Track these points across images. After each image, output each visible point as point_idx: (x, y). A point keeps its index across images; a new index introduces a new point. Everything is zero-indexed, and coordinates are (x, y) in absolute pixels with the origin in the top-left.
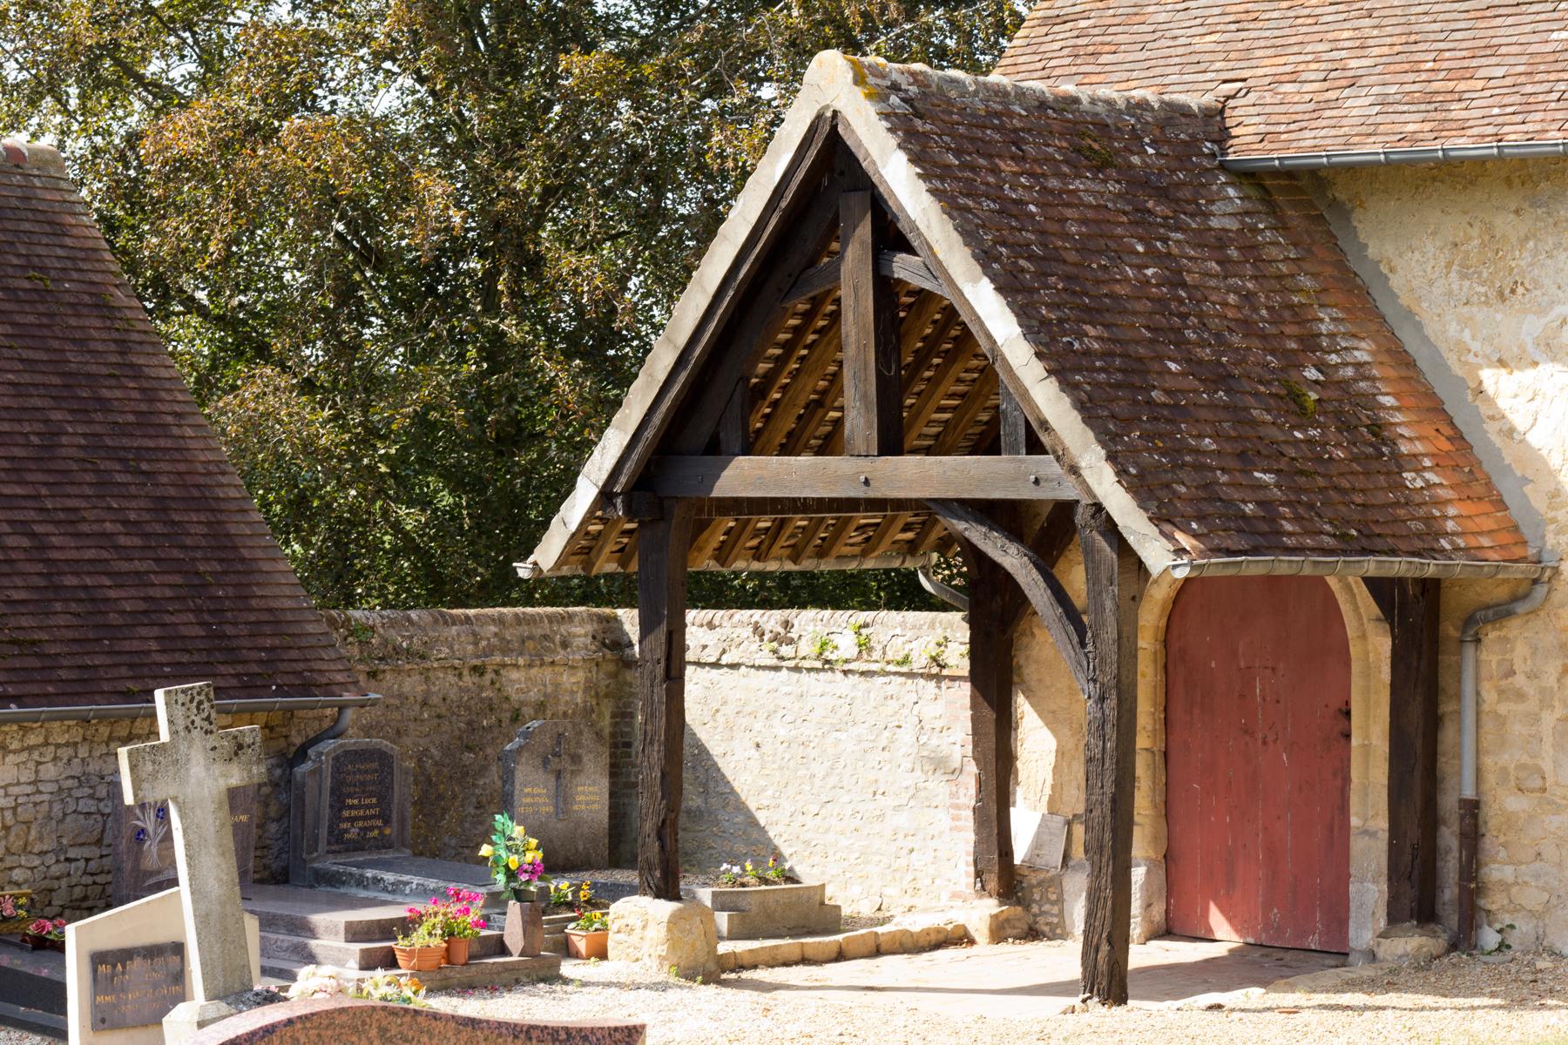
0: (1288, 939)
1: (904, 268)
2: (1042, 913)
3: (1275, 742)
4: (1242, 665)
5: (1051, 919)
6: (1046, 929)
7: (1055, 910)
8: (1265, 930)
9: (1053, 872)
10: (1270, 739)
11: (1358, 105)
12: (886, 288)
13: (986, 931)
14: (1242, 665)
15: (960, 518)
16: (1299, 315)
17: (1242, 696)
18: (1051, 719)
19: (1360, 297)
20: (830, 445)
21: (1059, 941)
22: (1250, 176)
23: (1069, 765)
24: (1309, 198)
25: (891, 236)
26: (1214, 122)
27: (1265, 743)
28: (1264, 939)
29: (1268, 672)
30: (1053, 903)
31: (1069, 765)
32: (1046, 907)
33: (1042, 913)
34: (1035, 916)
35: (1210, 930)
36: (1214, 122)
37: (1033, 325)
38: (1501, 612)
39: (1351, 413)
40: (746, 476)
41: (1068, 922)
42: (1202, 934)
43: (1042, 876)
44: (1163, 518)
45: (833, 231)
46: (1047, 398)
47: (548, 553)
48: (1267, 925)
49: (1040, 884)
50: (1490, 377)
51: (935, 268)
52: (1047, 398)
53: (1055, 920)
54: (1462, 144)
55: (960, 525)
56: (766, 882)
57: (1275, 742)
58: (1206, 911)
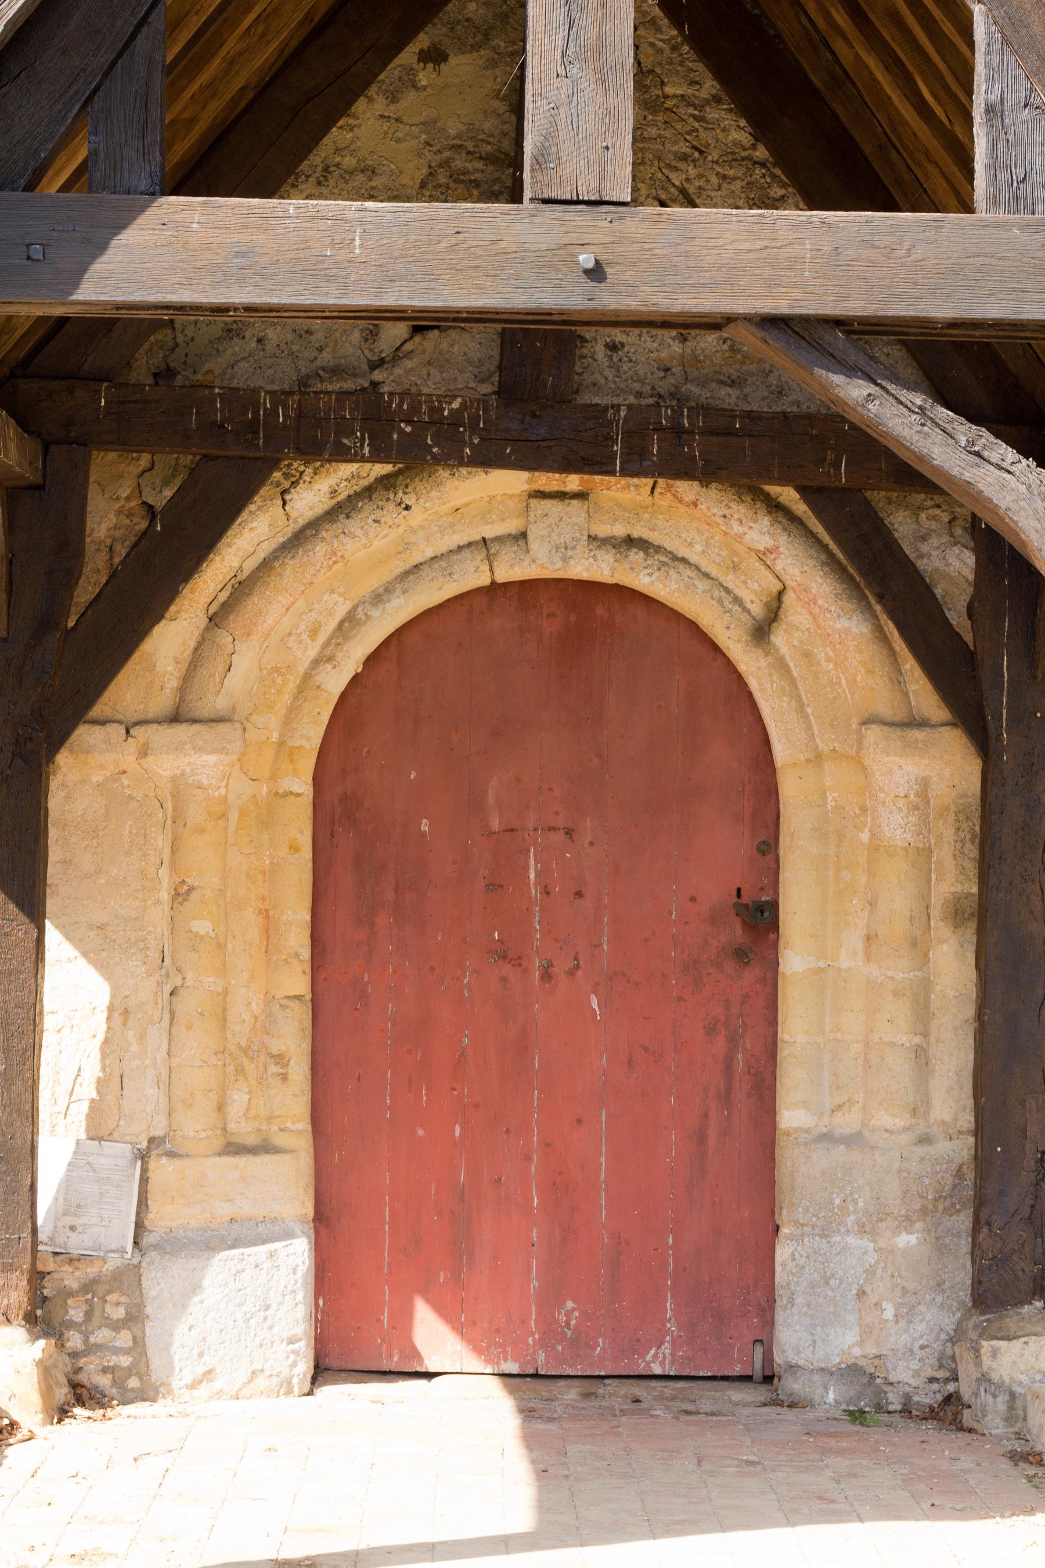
0: (601, 1356)
2: (90, 1349)
3: (571, 973)
4: (496, 825)
5: (114, 1360)
6: (104, 1381)
7: (124, 1339)
8: (543, 1343)
9: (114, 1262)
10: (561, 966)
13: (35, 1399)
14: (496, 825)
15: (851, 370)
17: (494, 887)
18: (99, 951)
21: (148, 1403)
23: (142, 1037)
27: (547, 975)
28: (542, 1362)
29: (558, 837)
30: (117, 1326)
31: (142, 1037)
32: (101, 1336)
33: (90, 1349)
34: (74, 1355)
35: (416, 1355)
41: (156, 1361)
42: (394, 1363)
43: (92, 1271)
48: (550, 1334)
49: (88, 1287)
53: (125, 1361)
55: (853, 391)
57: (571, 973)
58: (405, 1319)
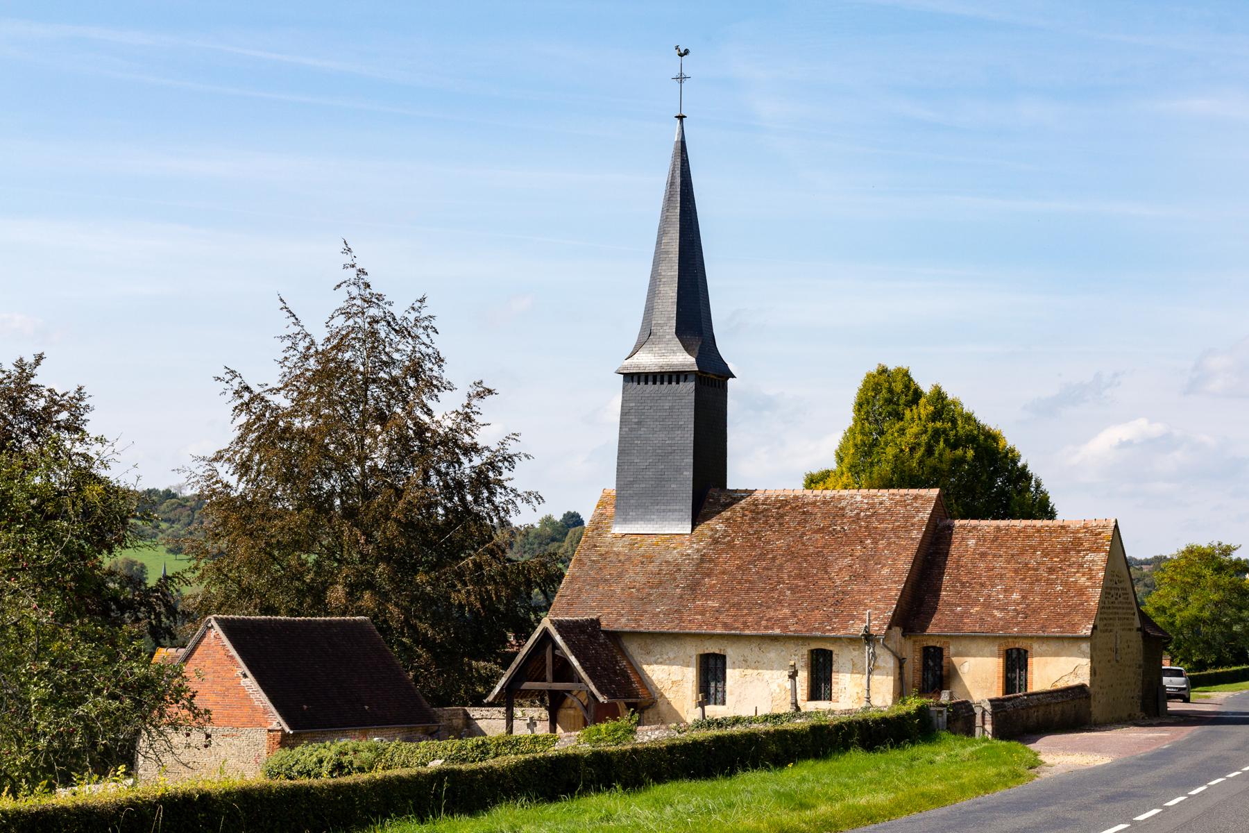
1: (557, 652)
11: (623, 620)
12: (554, 656)
16: (615, 657)
19: (624, 654)
20: (544, 680)
22: (605, 632)
24: (615, 637)
25: (555, 646)
26: (597, 622)
36: (597, 622)
37: (581, 664)
38: (648, 707)
39: (624, 673)
40: (527, 685)
44: (602, 694)
45: (545, 648)
46: (583, 674)
47: (490, 698)
50: (645, 667)
51: (563, 652)
52: (583, 674)
54: (642, 630)
56: (291, 778)
